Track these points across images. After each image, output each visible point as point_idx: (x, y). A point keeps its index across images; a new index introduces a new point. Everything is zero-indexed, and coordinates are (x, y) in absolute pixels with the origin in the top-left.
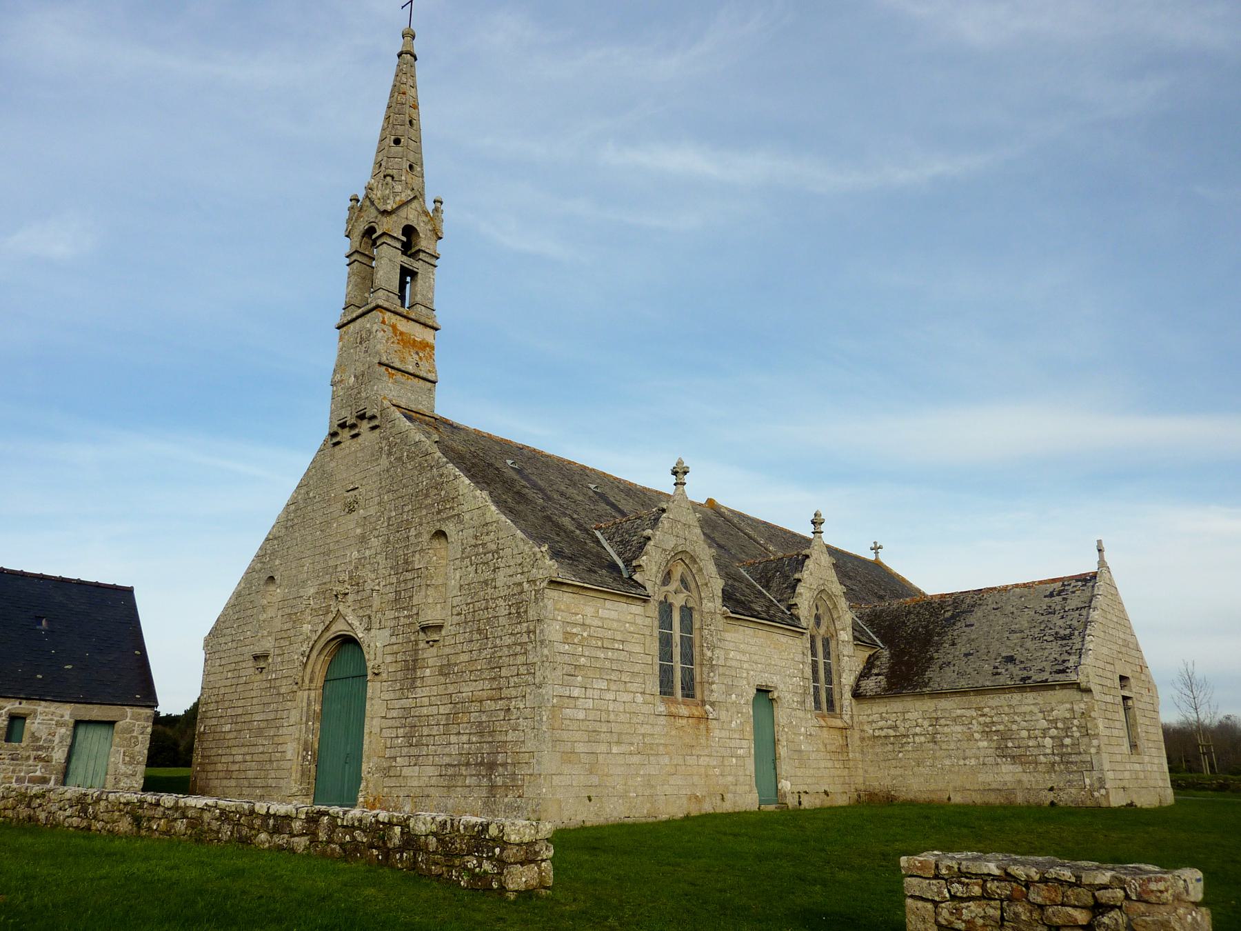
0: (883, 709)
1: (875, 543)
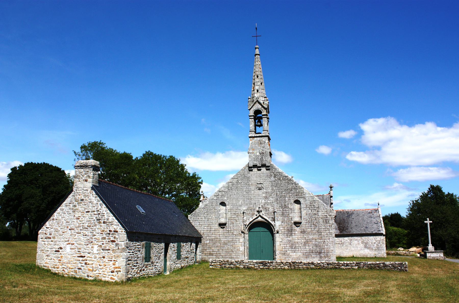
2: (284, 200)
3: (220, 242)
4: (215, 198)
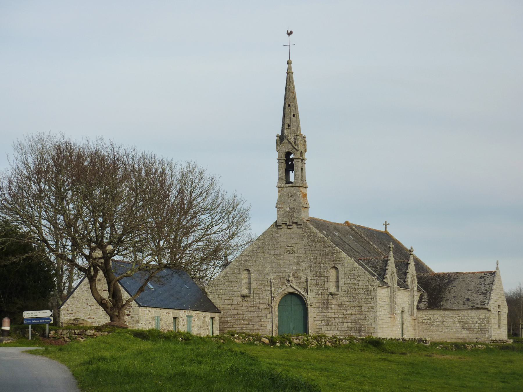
0: (426, 313)
1: (386, 222)
2: (318, 267)
3: (244, 319)
4: (238, 264)
